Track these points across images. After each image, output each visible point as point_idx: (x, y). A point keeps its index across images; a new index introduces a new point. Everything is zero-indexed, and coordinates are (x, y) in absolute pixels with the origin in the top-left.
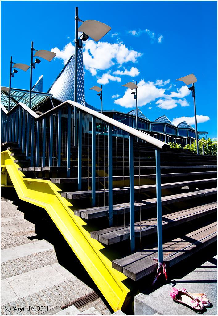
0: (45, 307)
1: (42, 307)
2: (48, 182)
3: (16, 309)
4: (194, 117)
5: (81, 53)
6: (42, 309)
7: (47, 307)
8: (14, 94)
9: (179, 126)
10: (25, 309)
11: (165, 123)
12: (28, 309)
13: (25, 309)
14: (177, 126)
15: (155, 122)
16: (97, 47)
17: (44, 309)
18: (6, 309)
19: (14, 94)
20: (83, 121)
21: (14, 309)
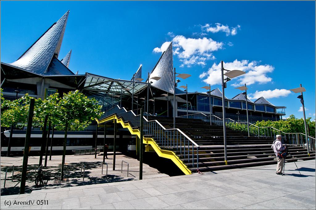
0: (45, 201)
1: (42, 201)
2: (151, 139)
3: (16, 203)
5: (171, 49)
7: (47, 201)
8: (124, 83)
11: (242, 101)
14: (254, 102)
15: (232, 100)
16: (187, 43)
18: (6, 203)
19: (124, 83)
20: (212, 105)
21: (14, 203)
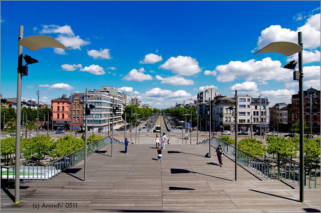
0: (74, 204)
3: (44, 206)
4: (305, 89)
6: (71, 206)
9: (238, 165)
10: (53, 206)
12: (57, 206)
13: (53, 206)
17: (73, 207)
18: (34, 206)
